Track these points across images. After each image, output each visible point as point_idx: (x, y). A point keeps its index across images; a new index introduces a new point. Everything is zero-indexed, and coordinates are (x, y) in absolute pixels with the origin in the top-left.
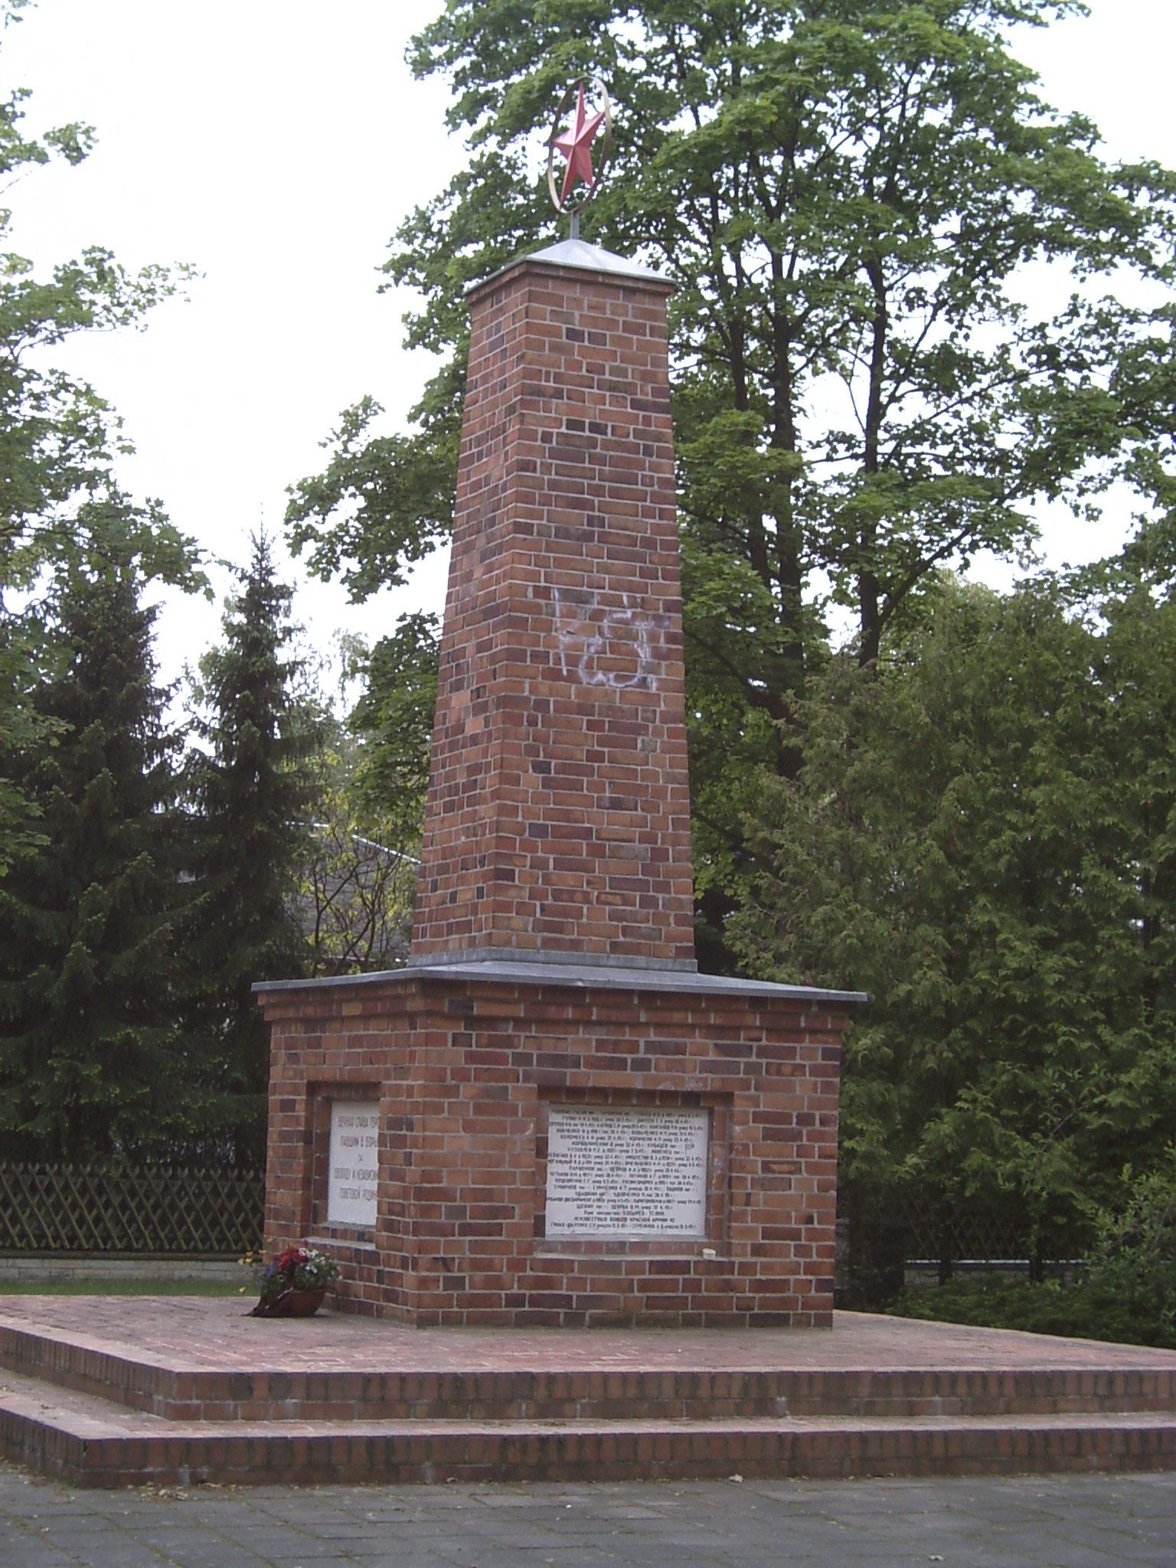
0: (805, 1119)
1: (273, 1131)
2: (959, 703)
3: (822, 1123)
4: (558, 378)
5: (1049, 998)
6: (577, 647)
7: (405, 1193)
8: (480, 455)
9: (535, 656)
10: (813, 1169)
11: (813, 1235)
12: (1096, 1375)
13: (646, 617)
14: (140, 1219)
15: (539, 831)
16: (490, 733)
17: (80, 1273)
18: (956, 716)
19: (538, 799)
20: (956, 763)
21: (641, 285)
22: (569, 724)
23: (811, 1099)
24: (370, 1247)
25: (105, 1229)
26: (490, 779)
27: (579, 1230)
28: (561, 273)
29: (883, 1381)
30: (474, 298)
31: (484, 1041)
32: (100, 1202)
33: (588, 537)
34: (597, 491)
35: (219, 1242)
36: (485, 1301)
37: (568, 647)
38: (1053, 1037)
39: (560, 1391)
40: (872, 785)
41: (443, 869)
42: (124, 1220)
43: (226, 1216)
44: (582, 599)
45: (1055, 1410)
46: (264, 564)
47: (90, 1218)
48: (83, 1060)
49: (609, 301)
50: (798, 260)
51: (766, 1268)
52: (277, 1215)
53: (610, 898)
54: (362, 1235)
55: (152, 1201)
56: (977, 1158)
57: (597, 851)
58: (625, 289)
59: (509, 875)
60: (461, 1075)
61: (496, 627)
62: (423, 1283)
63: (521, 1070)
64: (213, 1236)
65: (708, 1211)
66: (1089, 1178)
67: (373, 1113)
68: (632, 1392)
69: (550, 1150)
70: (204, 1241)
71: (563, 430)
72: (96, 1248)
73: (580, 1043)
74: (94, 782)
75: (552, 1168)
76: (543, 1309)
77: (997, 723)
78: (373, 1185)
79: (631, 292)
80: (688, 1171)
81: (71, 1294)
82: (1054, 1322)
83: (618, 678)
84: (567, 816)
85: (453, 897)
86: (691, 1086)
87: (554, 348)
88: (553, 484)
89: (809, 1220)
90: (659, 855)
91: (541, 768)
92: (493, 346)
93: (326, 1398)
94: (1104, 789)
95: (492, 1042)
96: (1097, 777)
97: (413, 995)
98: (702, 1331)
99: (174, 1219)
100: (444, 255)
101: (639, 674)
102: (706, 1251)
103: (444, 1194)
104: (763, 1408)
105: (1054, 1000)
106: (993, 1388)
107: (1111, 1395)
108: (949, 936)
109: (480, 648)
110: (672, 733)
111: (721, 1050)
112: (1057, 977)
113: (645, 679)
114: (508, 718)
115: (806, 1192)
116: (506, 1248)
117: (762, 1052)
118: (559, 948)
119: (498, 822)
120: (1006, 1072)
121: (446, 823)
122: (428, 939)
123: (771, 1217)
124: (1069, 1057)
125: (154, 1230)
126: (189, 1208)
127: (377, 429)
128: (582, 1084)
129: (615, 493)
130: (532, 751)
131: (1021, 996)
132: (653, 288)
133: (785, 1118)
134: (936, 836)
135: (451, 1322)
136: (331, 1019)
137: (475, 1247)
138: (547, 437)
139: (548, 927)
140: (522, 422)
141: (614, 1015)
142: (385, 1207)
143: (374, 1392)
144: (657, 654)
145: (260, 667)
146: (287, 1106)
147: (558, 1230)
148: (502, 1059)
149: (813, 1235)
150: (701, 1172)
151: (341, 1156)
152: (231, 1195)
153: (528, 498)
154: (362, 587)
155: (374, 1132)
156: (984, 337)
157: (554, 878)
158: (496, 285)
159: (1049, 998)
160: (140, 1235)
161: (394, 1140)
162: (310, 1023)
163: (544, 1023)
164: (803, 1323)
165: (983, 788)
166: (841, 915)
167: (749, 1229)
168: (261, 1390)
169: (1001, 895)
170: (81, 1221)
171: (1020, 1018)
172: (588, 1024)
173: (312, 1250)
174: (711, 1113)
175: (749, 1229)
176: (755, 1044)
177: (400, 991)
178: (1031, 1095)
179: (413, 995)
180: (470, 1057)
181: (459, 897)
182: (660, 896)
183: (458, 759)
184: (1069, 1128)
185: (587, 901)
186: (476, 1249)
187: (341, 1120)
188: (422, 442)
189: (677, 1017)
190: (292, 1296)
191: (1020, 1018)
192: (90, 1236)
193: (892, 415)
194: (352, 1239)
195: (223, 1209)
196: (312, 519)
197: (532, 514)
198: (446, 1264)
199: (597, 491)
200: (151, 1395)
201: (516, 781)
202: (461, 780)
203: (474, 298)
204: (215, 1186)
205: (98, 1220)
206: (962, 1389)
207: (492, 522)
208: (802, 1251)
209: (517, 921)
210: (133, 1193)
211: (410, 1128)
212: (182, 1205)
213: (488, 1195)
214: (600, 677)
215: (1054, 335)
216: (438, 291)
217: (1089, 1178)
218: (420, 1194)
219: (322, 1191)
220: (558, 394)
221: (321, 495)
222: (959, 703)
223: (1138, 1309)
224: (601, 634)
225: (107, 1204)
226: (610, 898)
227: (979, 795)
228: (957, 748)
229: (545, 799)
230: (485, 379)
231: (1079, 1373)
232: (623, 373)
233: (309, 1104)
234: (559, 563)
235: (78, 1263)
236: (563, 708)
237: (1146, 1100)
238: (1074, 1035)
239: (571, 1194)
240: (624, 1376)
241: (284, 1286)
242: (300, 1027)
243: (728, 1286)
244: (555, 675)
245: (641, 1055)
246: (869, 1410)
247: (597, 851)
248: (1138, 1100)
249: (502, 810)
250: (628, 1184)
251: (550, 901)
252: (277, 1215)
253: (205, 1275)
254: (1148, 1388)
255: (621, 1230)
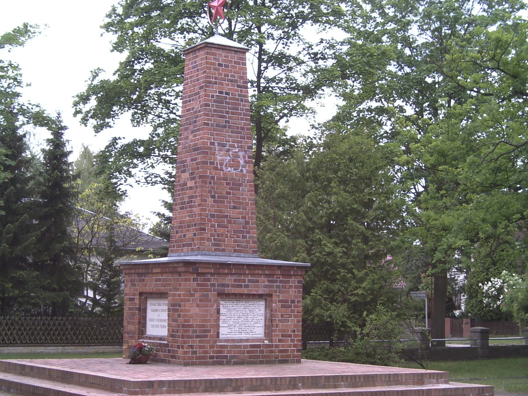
0: (293, 302)
1: (126, 308)
2: (308, 170)
3: (298, 303)
4: (216, 78)
5: (339, 261)
6: (223, 160)
7: (178, 326)
8: (190, 101)
9: (210, 162)
10: (295, 316)
11: (295, 336)
12: (385, 375)
13: (242, 151)
14: (25, 333)
15: (213, 216)
16: (197, 186)
17: (6, 351)
18: (308, 174)
19: (212, 206)
20: (308, 189)
21: (239, 50)
22: (221, 184)
23: (294, 295)
24: (166, 342)
25: (14, 337)
26: (198, 201)
27: (229, 336)
28: (216, 46)
29: (327, 378)
30: (186, 52)
31: (202, 280)
32: (12, 328)
33: (225, 127)
34: (227, 113)
35: (50, 340)
36: (204, 358)
37: (220, 160)
38: (339, 273)
39: (239, 384)
40: (282, 196)
41: (180, 227)
42: (20, 333)
43: (42, 331)
44: (224, 145)
45: (374, 386)
46: (60, 119)
47: (9, 333)
48: (5, 282)
49: (230, 55)
50: (237, 25)
51: (282, 346)
52: (128, 333)
53: (233, 236)
54: (161, 339)
55: (29, 327)
56: (317, 311)
57: (229, 222)
58: (234, 51)
59: (204, 229)
60: (196, 290)
61: (198, 154)
62: (185, 353)
63: (212, 288)
64: (48, 338)
65: (265, 329)
66: (351, 316)
67: (166, 302)
68: (259, 383)
69: (221, 312)
70: (45, 340)
71: (217, 94)
72: (11, 343)
73: (229, 280)
74: (8, 191)
75: (221, 317)
76: (220, 359)
77: (320, 176)
78: (166, 324)
79: (236, 52)
80: (260, 318)
81: (60, 358)
82: (344, 360)
83: (234, 169)
84: (221, 211)
85: (185, 236)
86: (261, 292)
87: (214, 69)
88: (215, 111)
89: (294, 331)
90: (247, 223)
91: (213, 197)
92: (193, 67)
93: (174, 387)
94: (354, 197)
95: (204, 280)
96: (351, 193)
97: (181, 267)
98: (264, 365)
99: (36, 333)
100: (121, 21)
101: (240, 168)
102: (265, 341)
103: (191, 326)
104: (295, 387)
105: (340, 262)
106: (358, 379)
107: (390, 381)
108: (306, 242)
109: (192, 160)
110: (250, 186)
111: (269, 281)
112: (341, 254)
113: (242, 170)
114: (203, 182)
115: (293, 323)
116: (209, 341)
117: (281, 282)
118: (219, 251)
119: (201, 213)
120: (325, 284)
121: (181, 213)
122: (175, 248)
123: (283, 331)
124: (344, 280)
125: (30, 337)
126: (41, 329)
127: (102, 77)
128: (230, 292)
129: (233, 113)
130: (210, 192)
131: (329, 260)
132: (242, 50)
133: (287, 301)
134: (303, 211)
135: (193, 364)
136: (149, 273)
137: (200, 342)
138: (213, 96)
139: (216, 245)
140: (205, 92)
141: (239, 272)
142: (171, 330)
143: (187, 385)
144: (246, 162)
145: (59, 153)
146: (132, 300)
147: (223, 336)
148: (206, 285)
149: (295, 336)
150: (263, 318)
151: (150, 315)
152: (54, 325)
153: (207, 115)
154: (98, 129)
155: (166, 308)
156: (293, 49)
157: (217, 230)
158: (195, 49)
159: (339, 261)
160: (25, 339)
161: (174, 310)
162: (140, 275)
163: (219, 274)
164: (293, 362)
165: (316, 197)
166: (274, 236)
167: (277, 335)
168: (156, 386)
169: (321, 228)
170: (6, 334)
171: (329, 268)
172: (232, 274)
173: (146, 343)
174: (266, 300)
175: (277, 335)
176: (278, 279)
177: (176, 265)
178: (332, 291)
179: (181, 267)
180: (198, 285)
181: (187, 236)
182: (248, 235)
183: (185, 194)
184: (344, 301)
185: (227, 237)
186: (194, 341)
187: (151, 304)
188: (118, 81)
189: (257, 272)
190: (140, 357)
191: (329, 268)
192: (9, 339)
193: (265, 74)
194: (157, 340)
195: (51, 329)
196: (81, 106)
197: (209, 120)
198: (192, 347)
199: (227, 113)
200: (122, 388)
201: (206, 201)
202: (186, 200)
203: (186, 52)
204: (49, 322)
205: (11, 334)
206: (349, 380)
207: (195, 122)
208: (292, 341)
209: (207, 243)
210: (22, 325)
211: (180, 306)
212: (38, 328)
213: (203, 326)
214: (229, 169)
215: (316, 49)
216: (119, 33)
217: (351, 316)
218: (183, 326)
219: (144, 325)
220: (216, 83)
221: (84, 99)
222: (308, 170)
223: (368, 355)
224: (229, 156)
225: (14, 329)
226: (233, 236)
227: (315, 199)
228: (309, 184)
229: (214, 206)
230: (191, 77)
231: (381, 375)
232: (234, 77)
233: (140, 299)
234: (217, 135)
235: (5, 348)
236: (219, 179)
237: (369, 292)
238: (346, 272)
239: (226, 325)
240: (257, 379)
241: (139, 355)
242: (136, 276)
243: (272, 351)
244: (216, 169)
245: (247, 283)
246: (324, 387)
247: (229, 222)
248: (367, 292)
249: (202, 210)
250: (243, 322)
251: (216, 237)
252: (128, 333)
253: (46, 351)
254: (399, 378)
255: (240, 336)
